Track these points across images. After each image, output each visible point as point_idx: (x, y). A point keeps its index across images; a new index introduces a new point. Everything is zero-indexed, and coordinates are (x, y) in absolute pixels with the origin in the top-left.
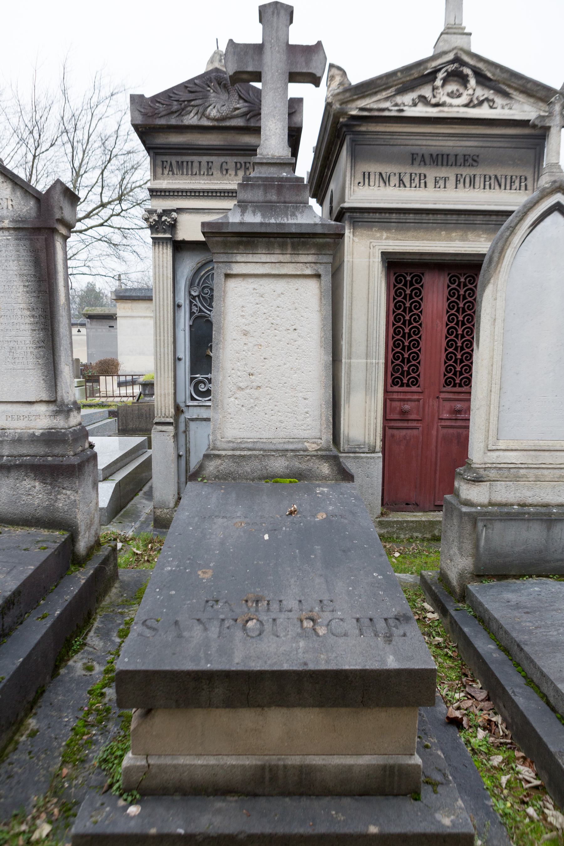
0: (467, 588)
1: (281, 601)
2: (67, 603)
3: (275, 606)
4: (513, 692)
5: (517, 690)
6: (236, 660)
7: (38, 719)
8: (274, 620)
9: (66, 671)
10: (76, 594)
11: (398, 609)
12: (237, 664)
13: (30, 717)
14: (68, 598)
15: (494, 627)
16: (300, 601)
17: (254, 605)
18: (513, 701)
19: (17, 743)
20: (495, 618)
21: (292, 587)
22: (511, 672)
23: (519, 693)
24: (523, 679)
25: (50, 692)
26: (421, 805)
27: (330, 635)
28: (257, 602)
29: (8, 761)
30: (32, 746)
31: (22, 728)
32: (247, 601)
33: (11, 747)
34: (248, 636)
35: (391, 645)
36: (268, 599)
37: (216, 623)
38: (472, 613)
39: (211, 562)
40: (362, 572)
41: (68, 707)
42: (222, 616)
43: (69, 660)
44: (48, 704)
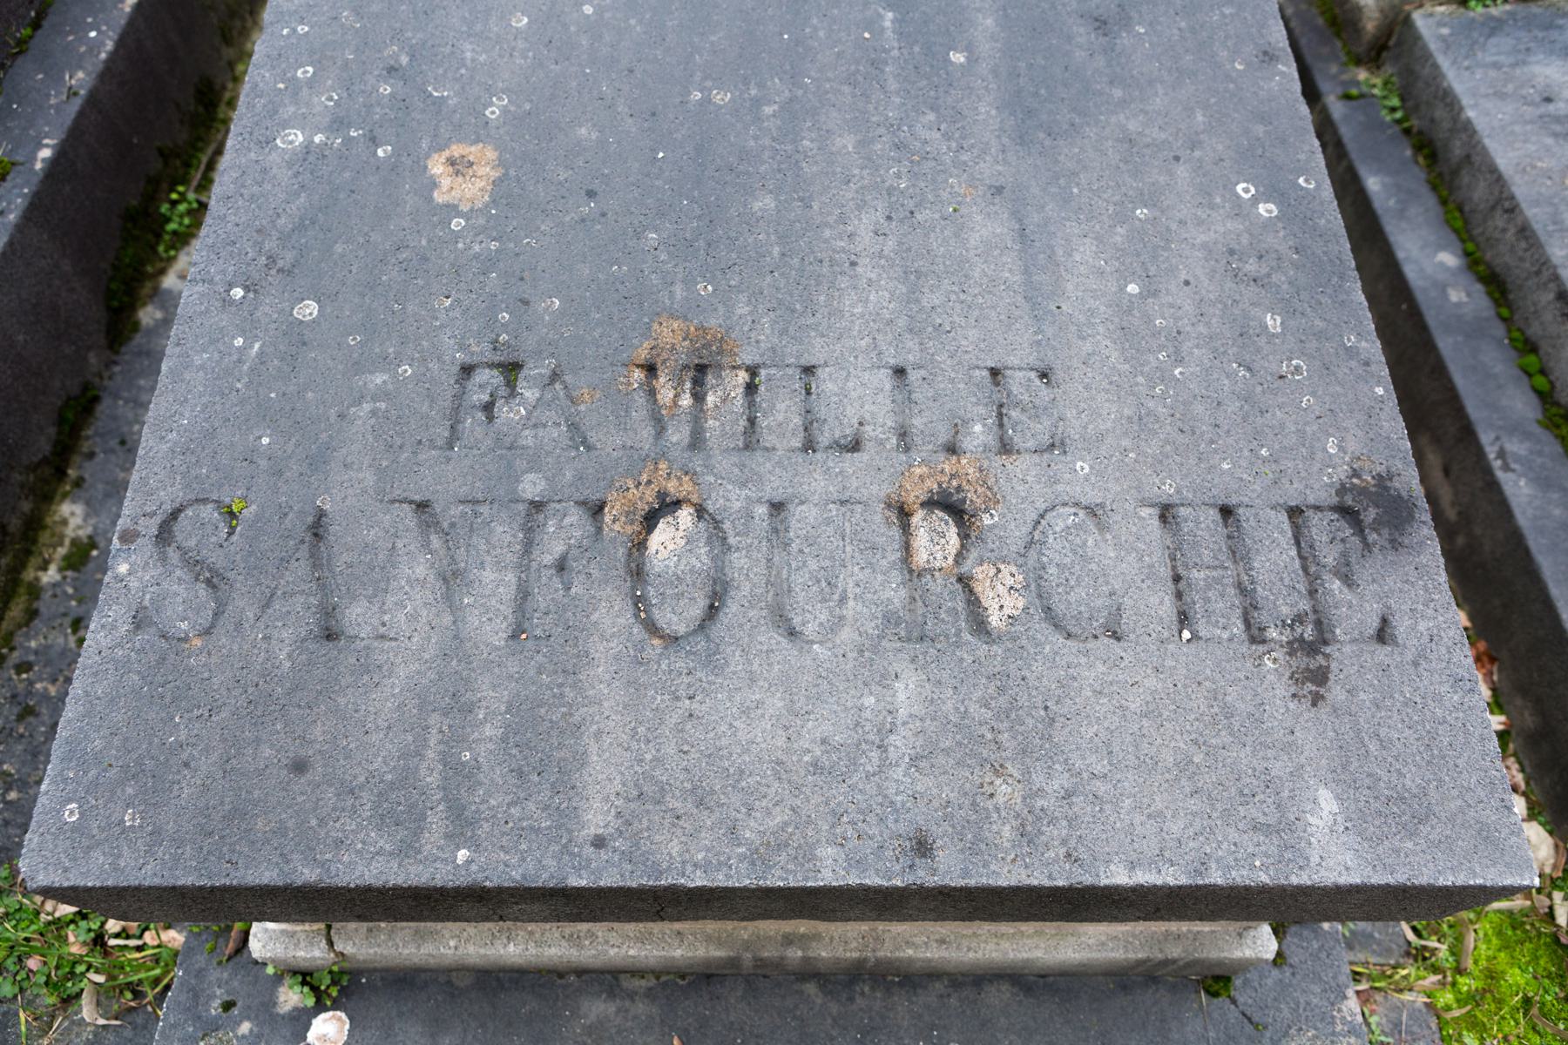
0: (1407, 21)
1: (809, 370)
2: (76, 104)
3: (782, 412)
4: (1501, 454)
5: (1514, 446)
6: (596, 818)
7: (88, 503)
8: (777, 507)
9: (159, 315)
10: (113, 55)
11: (1353, 446)
12: (599, 842)
13: (65, 496)
14: (80, 79)
15: (1478, 193)
16: (900, 372)
17: (686, 401)
18: (1493, 486)
19: (35, 591)
20: (1493, 170)
21: (865, 270)
22: (1499, 368)
23: (1518, 459)
24: (1534, 400)
25: (117, 396)
26: (1233, 1013)
27: (1041, 629)
28: (699, 373)
29: (16, 656)
30: (80, 602)
31: (44, 537)
32: (651, 369)
33: (16, 611)
34: (652, 628)
35: (1324, 710)
36: (748, 357)
37: (505, 533)
38: (1399, 115)
39: (490, 91)
40: (1182, 171)
41: (128, 537)
42: (532, 486)
43: (162, 272)
44: (114, 443)
